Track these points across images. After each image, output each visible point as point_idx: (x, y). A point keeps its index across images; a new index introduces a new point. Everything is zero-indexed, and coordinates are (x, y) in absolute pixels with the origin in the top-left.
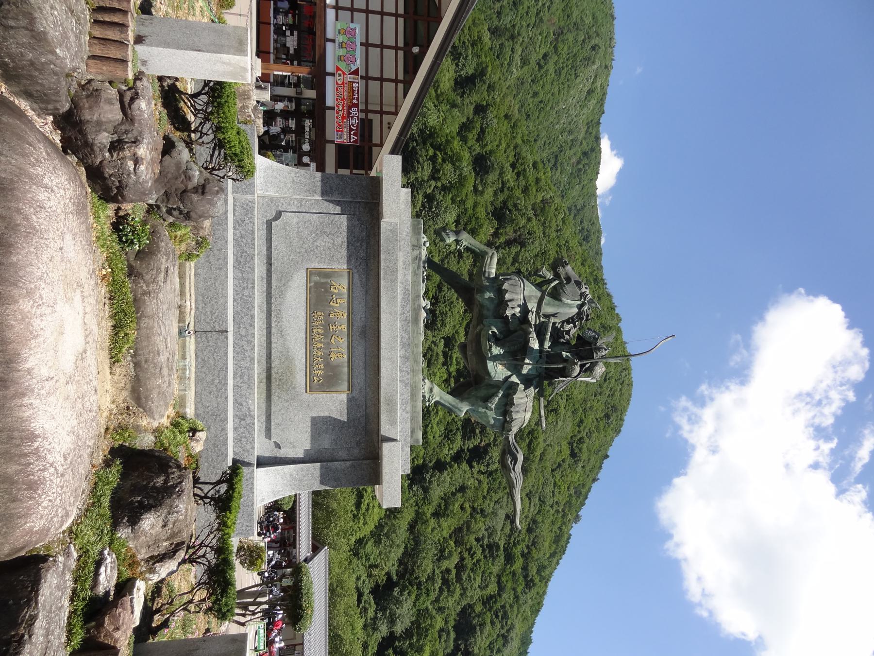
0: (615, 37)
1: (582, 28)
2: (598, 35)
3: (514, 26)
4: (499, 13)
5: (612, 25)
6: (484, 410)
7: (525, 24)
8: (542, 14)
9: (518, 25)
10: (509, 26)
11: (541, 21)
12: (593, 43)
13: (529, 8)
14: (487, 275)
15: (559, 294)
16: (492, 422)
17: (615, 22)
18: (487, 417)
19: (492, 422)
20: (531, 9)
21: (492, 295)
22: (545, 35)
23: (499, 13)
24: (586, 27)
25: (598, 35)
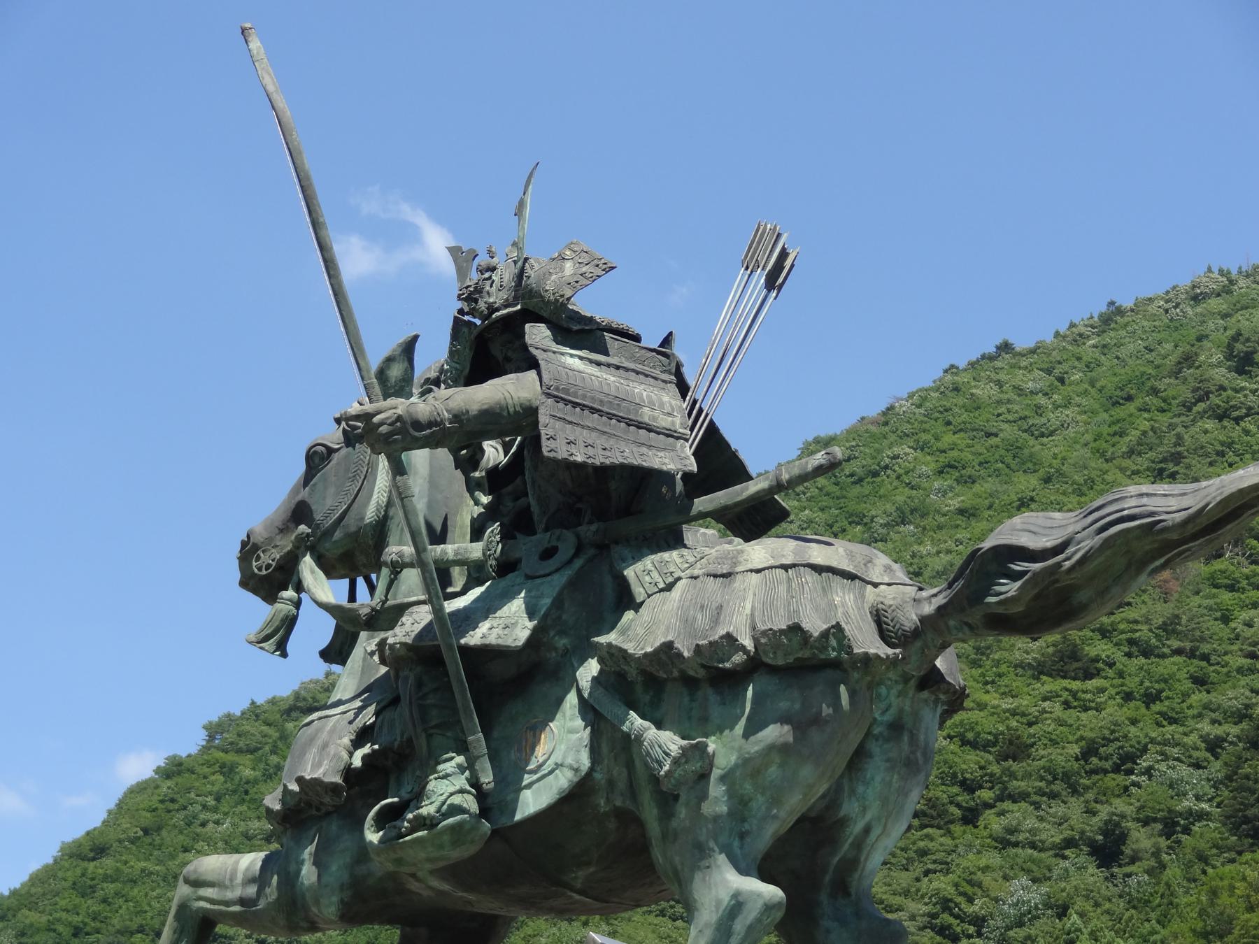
0: (1185, 282)
1: (1170, 439)
2: (1188, 360)
3: (1214, 746)
4: (1172, 825)
5: (1141, 306)
6: (716, 790)
7: (1198, 697)
8: (1143, 632)
9: (1205, 727)
10: (1216, 768)
11: (1169, 628)
12: (1221, 374)
13: (1128, 697)
14: (252, 890)
15: (355, 536)
16: (774, 733)
17: (1128, 303)
18: (750, 768)
19: (774, 733)
20: (1131, 683)
21: (308, 852)
22: (1226, 597)
23: (1172, 825)
24: (1165, 419)
25: (1188, 360)
